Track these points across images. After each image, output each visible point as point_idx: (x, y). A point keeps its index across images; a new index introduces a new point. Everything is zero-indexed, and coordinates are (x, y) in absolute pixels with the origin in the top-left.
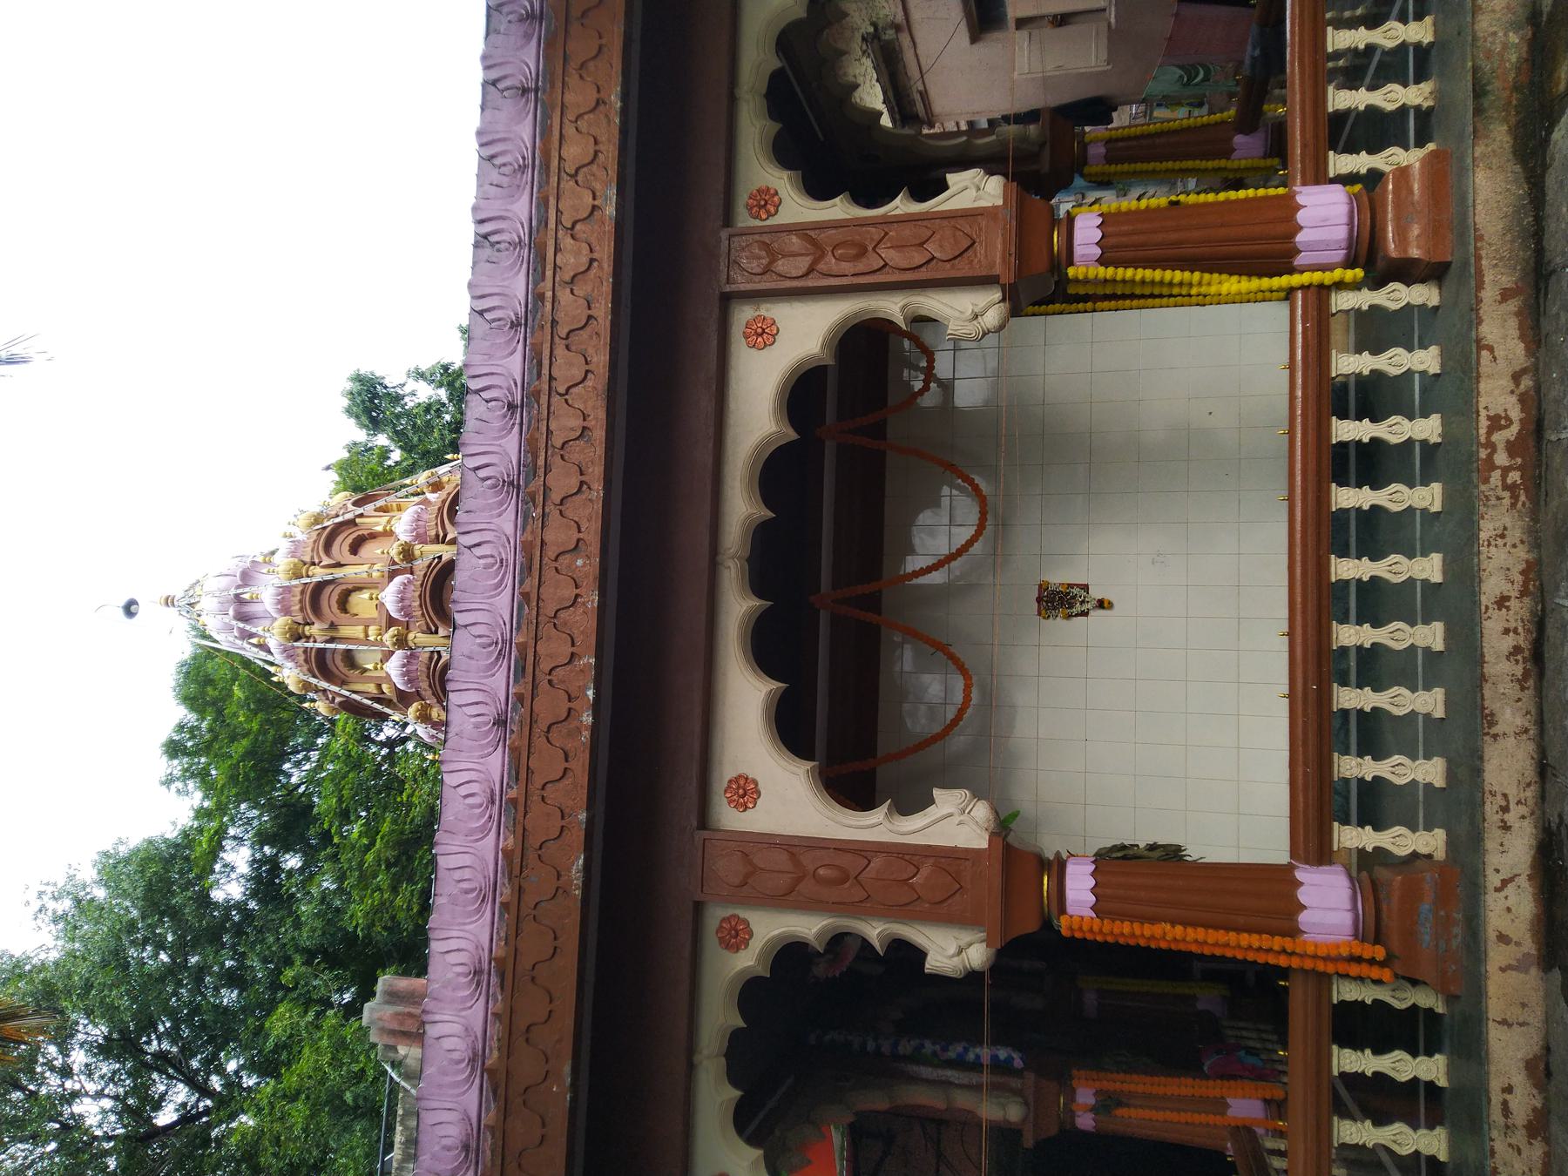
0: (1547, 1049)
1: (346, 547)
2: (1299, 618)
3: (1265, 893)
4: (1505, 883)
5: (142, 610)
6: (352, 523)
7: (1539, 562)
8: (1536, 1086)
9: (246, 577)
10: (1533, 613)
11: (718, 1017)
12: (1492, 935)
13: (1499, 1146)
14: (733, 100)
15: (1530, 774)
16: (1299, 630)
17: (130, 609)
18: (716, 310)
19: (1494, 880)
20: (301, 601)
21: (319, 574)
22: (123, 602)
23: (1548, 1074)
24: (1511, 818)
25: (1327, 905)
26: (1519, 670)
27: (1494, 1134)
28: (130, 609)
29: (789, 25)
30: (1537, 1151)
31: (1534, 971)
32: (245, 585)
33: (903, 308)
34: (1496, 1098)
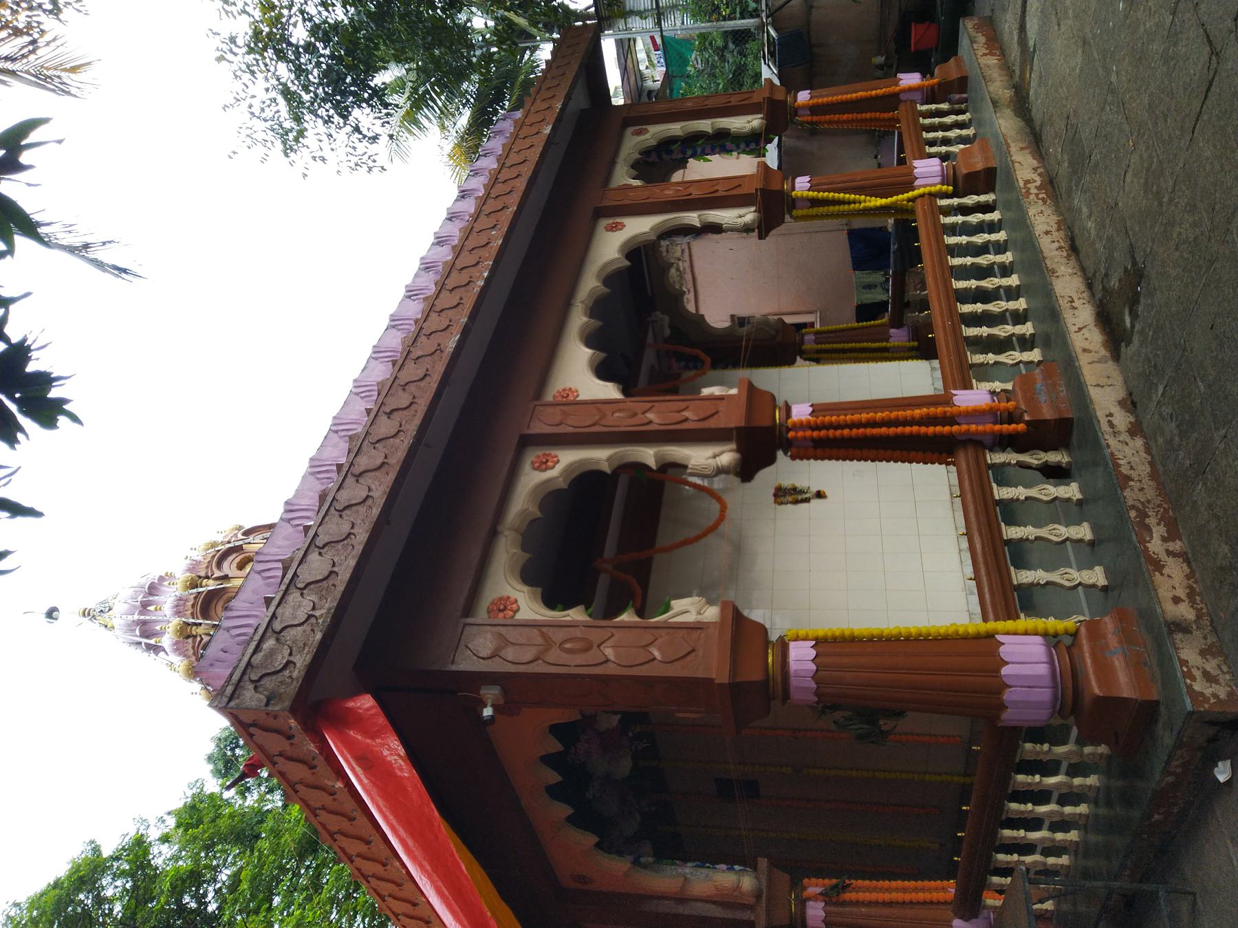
0: (1131, 394)
1: (234, 565)
2: (982, 566)
3: (979, 649)
4: (1080, 329)
5: (62, 615)
6: (238, 549)
7: (1065, 219)
8: (1128, 411)
9: (153, 589)
10: (1067, 236)
11: (590, 284)
12: (1079, 350)
13: (1112, 442)
14: (494, 533)
15: (1083, 288)
16: (983, 572)
17: (51, 614)
18: (512, 453)
19: (1073, 329)
20: (193, 606)
21: (211, 585)
22: (45, 610)
23: (1134, 404)
24: (1076, 304)
25: (1024, 653)
26: (1065, 254)
27: (1107, 437)
28: (51, 614)
29: (503, 899)
30: (1139, 442)
31: (1110, 363)
32: (151, 594)
33: (656, 455)
34: (1103, 422)
